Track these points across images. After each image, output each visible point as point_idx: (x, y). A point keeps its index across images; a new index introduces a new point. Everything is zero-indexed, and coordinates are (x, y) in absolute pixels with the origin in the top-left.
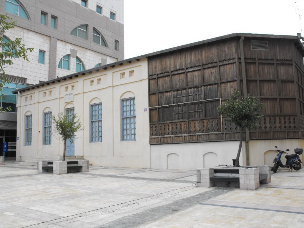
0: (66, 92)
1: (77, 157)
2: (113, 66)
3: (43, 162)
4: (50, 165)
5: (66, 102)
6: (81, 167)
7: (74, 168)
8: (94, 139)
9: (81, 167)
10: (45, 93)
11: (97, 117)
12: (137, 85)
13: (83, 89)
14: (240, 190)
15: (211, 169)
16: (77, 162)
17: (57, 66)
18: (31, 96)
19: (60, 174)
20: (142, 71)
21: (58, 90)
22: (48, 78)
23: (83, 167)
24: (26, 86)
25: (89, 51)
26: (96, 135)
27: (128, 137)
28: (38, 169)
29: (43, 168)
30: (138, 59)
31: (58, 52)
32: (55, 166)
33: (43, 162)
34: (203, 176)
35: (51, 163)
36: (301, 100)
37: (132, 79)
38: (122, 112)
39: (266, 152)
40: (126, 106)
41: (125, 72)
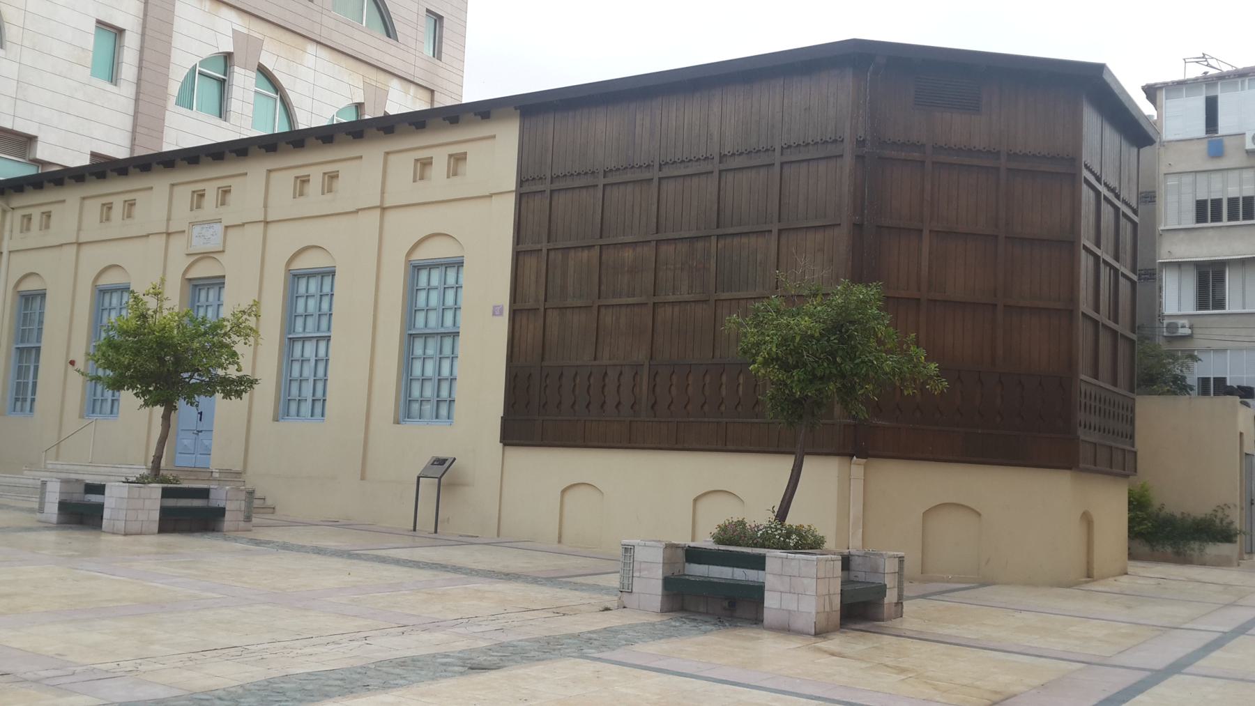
0: (196, 213)
1: (216, 475)
2: (417, 122)
3: (65, 482)
4: (94, 498)
5: (191, 251)
6: (221, 512)
7: (190, 513)
8: (293, 406)
9: (221, 512)
10: (109, 207)
11: (433, 317)
12: (476, 214)
13: (265, 206)
14: (226, 545)
15: (670, 547)
16: (204, 493)
17: (174, 100)
18: (48, 215)
19: (126, 535)
20: (497, 158)
21: (157, 198)
22: (127, 143)
23: (228, 516)
24: (29, 171)
25: (311, 48)
26: (301, 396)
27: (427, 408)
28: (41, 510)
29: (63, 506)
30: (485, 111)
31: (177, 41)
32: (113, 500)
33: (65, 482)
34: (640, 571)
35: (99, 489)
36: (1103, 318)
37: (458, 188)
38: (410, 310)
39: (935, 507)
40: (429, 289)
41: (465, 153)
